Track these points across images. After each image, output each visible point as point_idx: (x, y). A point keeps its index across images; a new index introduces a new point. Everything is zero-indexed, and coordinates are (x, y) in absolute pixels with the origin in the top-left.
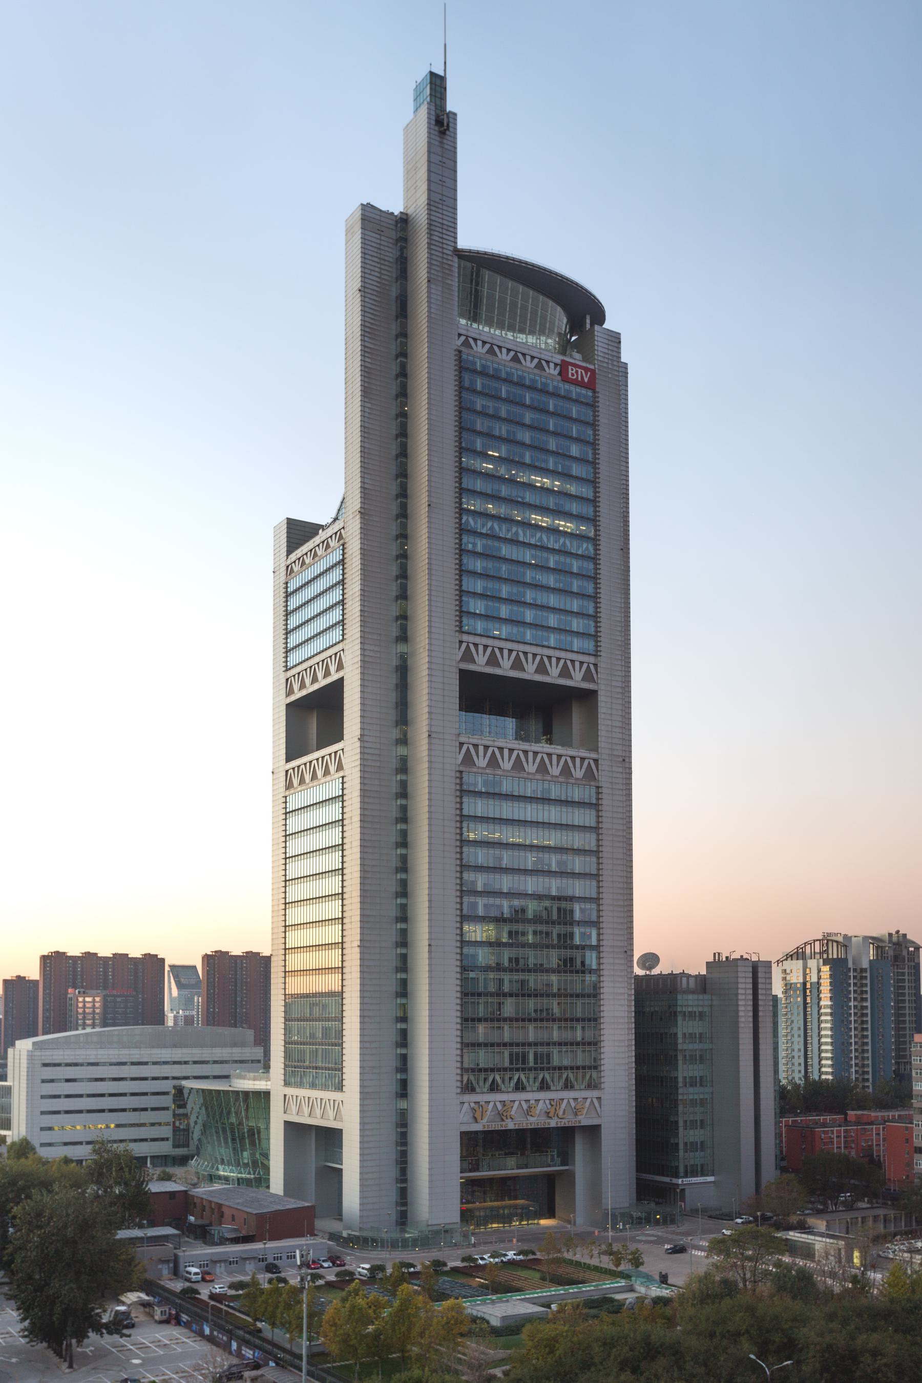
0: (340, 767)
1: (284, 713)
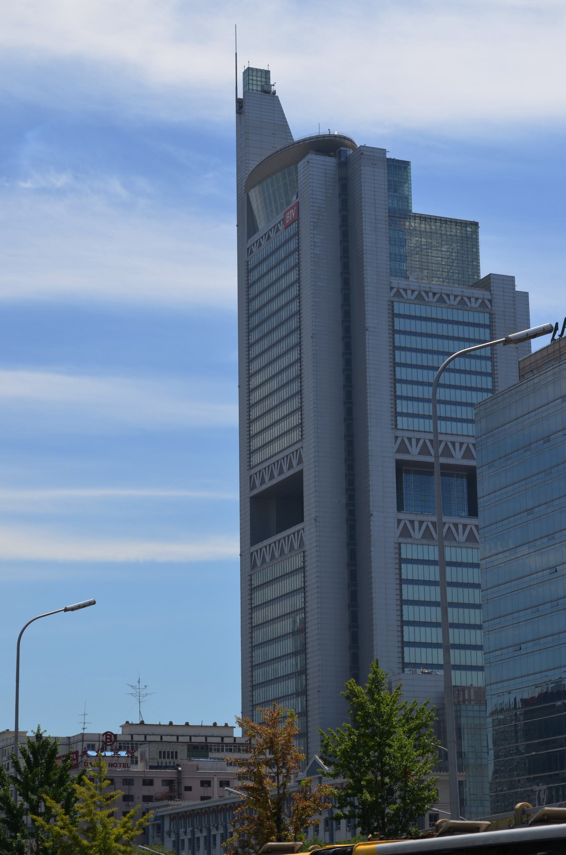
0: (302, 544)
1: (249, 504)
